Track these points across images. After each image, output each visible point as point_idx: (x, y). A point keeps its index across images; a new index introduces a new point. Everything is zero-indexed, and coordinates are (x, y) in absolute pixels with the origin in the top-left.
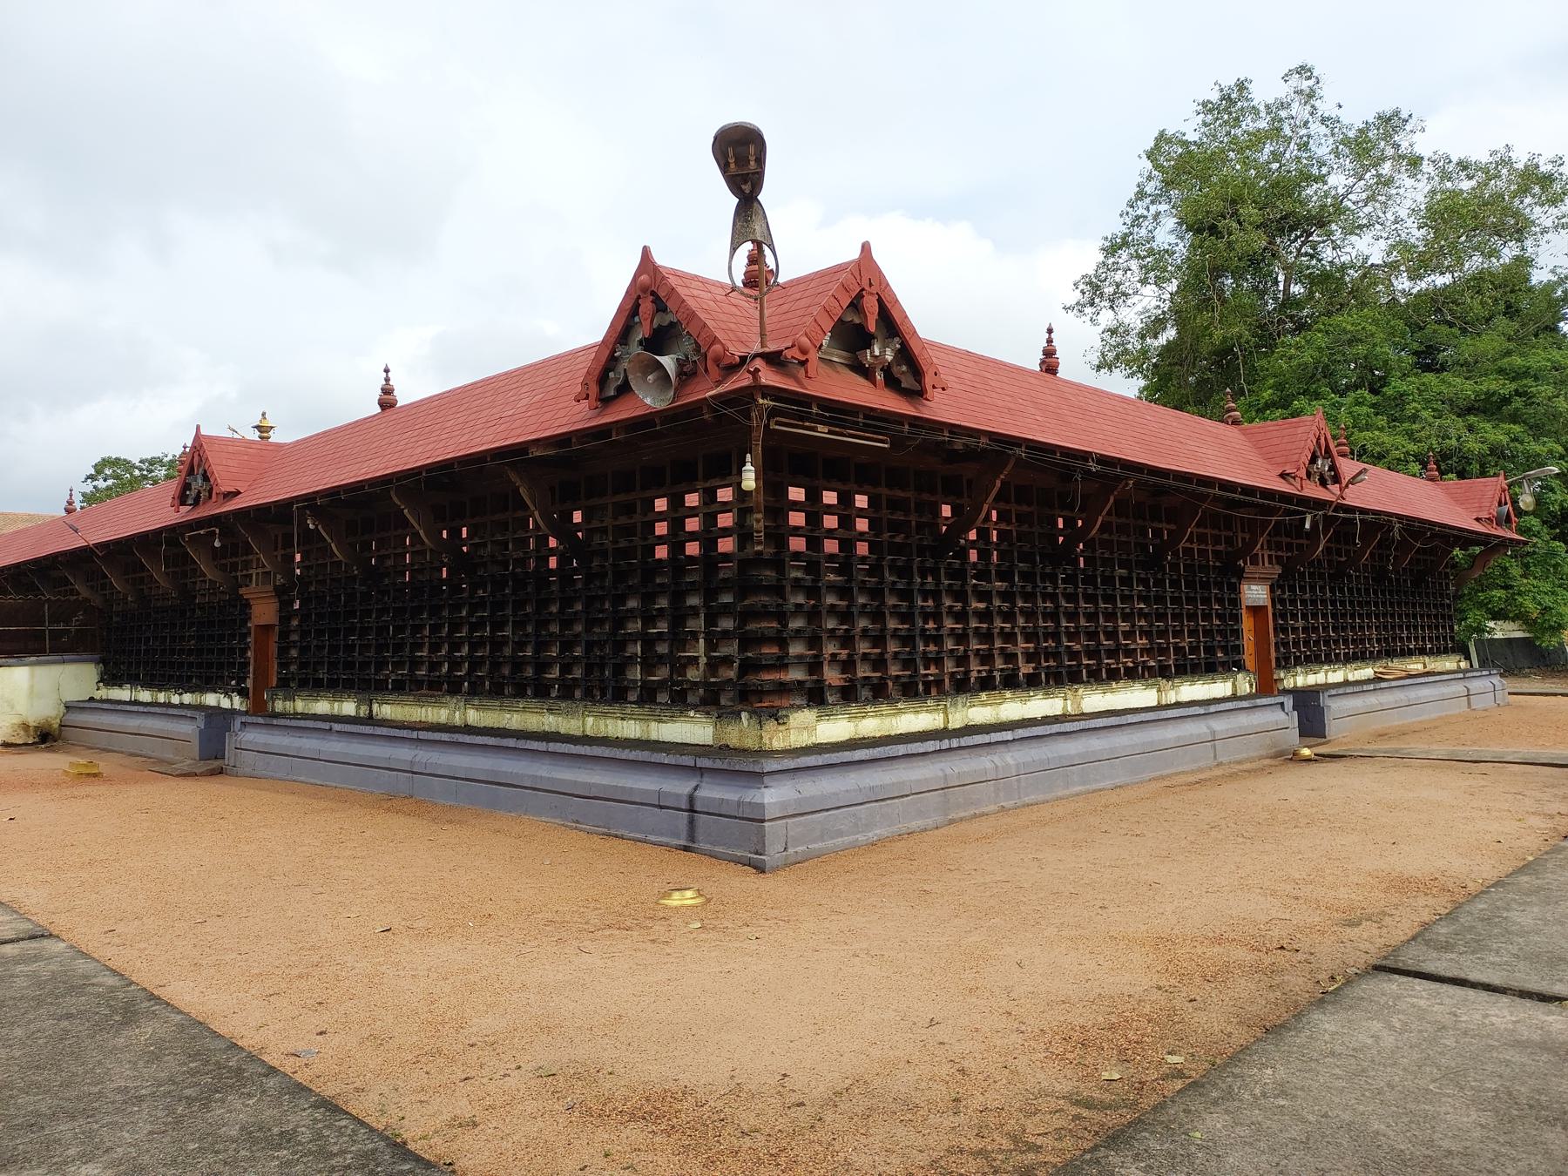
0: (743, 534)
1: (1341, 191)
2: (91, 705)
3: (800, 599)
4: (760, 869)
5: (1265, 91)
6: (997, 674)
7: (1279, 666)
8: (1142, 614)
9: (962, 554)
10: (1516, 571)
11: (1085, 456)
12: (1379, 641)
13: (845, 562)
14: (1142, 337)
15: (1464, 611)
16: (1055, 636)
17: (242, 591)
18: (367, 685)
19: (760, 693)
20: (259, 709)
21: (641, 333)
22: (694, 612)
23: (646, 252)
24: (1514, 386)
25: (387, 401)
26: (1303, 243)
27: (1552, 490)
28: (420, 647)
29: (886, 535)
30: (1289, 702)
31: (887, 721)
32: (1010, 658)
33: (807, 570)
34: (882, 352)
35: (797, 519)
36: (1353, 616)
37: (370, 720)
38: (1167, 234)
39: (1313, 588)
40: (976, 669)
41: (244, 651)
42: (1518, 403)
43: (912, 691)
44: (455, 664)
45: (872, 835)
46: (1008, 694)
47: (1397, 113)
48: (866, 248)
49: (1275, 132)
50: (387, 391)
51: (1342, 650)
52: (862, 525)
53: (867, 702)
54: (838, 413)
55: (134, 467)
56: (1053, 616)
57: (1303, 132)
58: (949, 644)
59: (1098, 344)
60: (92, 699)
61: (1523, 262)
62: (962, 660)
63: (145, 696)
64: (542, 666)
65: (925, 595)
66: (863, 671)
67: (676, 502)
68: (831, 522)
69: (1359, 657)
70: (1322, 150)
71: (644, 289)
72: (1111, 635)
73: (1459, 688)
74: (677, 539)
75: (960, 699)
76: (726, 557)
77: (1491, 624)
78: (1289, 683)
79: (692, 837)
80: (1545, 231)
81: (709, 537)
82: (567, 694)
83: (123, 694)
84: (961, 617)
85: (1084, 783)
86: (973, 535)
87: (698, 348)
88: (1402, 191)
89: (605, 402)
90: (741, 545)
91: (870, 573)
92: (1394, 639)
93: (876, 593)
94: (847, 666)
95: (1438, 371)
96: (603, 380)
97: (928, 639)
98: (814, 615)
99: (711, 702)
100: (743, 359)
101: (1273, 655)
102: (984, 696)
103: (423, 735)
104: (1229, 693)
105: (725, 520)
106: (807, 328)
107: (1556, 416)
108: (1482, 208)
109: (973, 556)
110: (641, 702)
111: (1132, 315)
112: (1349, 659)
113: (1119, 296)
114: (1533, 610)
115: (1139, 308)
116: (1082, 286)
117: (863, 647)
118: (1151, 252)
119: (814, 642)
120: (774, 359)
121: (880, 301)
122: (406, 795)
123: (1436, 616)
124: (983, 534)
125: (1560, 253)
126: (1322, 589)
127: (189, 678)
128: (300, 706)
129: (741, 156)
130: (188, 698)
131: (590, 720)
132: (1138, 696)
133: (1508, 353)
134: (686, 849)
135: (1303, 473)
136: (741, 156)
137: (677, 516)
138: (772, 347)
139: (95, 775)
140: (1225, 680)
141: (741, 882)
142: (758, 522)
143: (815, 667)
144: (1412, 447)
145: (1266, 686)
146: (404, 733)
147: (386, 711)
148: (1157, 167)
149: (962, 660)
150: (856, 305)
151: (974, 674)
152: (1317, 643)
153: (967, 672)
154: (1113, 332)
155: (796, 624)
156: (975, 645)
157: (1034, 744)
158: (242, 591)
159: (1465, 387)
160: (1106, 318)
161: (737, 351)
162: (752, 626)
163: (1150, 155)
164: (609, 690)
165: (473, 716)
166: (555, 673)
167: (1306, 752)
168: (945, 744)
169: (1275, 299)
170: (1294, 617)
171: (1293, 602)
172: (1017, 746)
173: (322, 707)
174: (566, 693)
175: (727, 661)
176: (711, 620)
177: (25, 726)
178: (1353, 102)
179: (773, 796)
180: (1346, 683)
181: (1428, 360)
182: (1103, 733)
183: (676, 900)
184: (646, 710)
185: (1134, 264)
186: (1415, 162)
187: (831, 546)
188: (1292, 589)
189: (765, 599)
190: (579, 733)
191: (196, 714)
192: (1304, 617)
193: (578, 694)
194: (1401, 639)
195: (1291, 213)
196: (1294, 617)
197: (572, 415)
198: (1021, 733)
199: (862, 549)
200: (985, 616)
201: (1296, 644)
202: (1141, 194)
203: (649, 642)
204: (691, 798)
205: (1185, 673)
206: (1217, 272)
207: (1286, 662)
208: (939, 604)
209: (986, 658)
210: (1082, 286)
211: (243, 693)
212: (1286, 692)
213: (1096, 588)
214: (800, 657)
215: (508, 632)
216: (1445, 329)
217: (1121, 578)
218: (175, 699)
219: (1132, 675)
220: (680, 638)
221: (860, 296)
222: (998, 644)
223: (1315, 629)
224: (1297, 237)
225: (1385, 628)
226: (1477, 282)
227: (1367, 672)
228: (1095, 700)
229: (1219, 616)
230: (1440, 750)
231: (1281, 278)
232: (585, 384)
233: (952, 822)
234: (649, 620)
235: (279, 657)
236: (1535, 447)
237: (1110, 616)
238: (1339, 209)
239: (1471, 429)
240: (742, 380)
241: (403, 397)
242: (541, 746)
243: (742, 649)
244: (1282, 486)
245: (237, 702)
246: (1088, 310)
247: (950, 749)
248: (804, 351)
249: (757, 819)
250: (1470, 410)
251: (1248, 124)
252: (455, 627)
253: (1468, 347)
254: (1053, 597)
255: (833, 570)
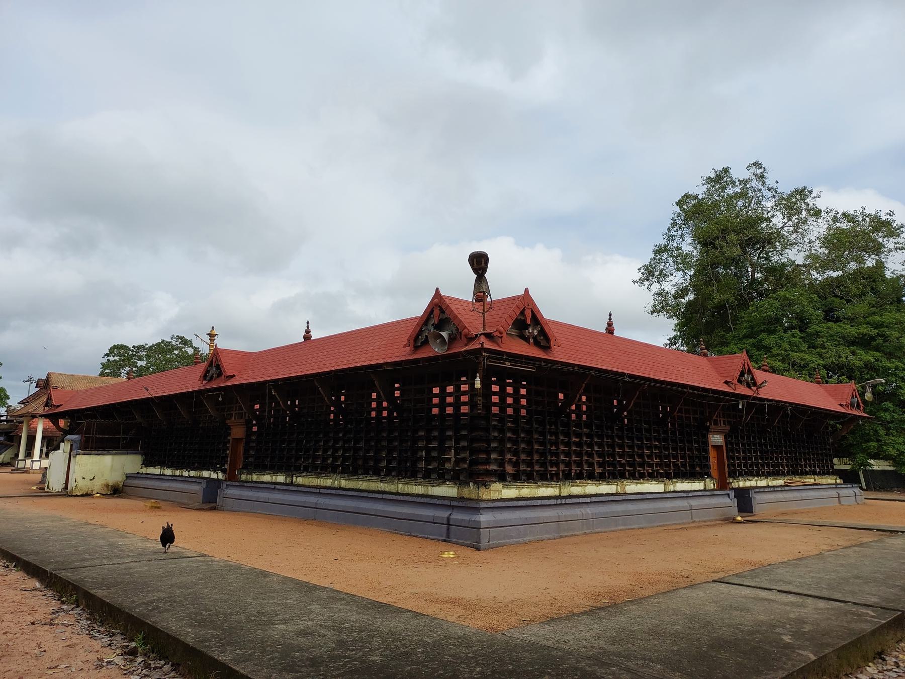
0: (472, 404)
1: (780, 225)
2: (138, 476)
3: (496, 434)
4: (478, 549)
5: (739, 173)
6: (584, 472)
7: (730, 476)
8: (656, 447)
9: (568, 416)
10: (882, 432)
11: (623, 374)
12: (787, 466)
13: (516, 416)
14: (675, 297)
15: (855, 454)
16: (613, 455)
17: (228, 421)
18: (290, 468)
19: (479, 474)
20: (232, 477)
21: (435, 320)
22: (450, 438)
23: (437, 290)
24: (876, 331)
25: (307, 337)
26: (761, 252)
27: (901, 388)
28: (317, 451)
29: (534, 407)
30: (732, 494)
31: (533, 490)
32: (591, 465)
33: (499, 421)
34: (533, 331)
35: (495, 399)
36: (772, 453)
37: (292, 484)
38: (688, 246)
39: (748, 438)
40: (574, 469)
41: (225, 451)
42: (880, 340)
43: (545, 478)
44: (335, 459)
45: (526, 539)
46: (589, 482)
47: (804, 189)
48: (527, 290)
49: (743, 194)
50: (308, 332)
51: (766, 469)
52: (523, 402)
53: (524, 481)
54: (515, 358)
55: (129, 350)
56: (612, 446)
57: (759, 194)
58: (562, 457)
59: (652, 302)
60: (138, 473)
61: (880, 266)
62: (568, 465)
63: (168, 472)
64: (378, 460)
65: (551, 434)
66: (523, 467)
67: (443, 390)
68: (510, 400)
69: (776, 474)
70: (769, 204)
71: (436, 305)
72: (641, 456)
73: (833, 493)
74: (442, 405)
75: (567, 483)
76: (465, 415)
77: (871, 461)
78: (735, 485)
79: (448, 536)
80: (890, 251)
81: (457, 405)
82: (389, 474)
83: (157, 471)
84: (568, 444)
85: (625, 525)
86: (573, 407)
87: (457, 329)
88: (811, 227)
89: (416, 348)
90: (471, 409)
91: (526, 423)
92: (797, 466)
93: (529, 432)
94: (516, 465)
95: (835, 322)
96: (416, 339)
97: (552, 454)
98: (501, 441)
99: (456, 478)
100: (476, 335)
101: (727, 470)
102: (578, 482)
103: (322, 491)
104: (702, 488)
105: (464, 398)
106: (503, 322)
107: (900, 348)
108: (860, 236)
109: (574, 416)
110: (424, 478)
111: (670, 286)
112: (769, 475)
113: (663, 277)
114: (893, 452)
115: (673, 283)
116: (642, 271)
117: (523, 457)
118: (680, 255)
119: (502, 453)
120: (489, 336)
121: (532, 311)
122: (313, 516)
123: (822, 455)
124: (579, 407)
125: (897, 263)
126: (754, 438)
127: (193, 463)
128: (255, 477)
129: (479, 262)
130: (192, 473)
131: (400, 486)
132: (654, 487)
133: (874, 313)
134: (445, 541)
135: (736, 381)
136: (479, 262)
137: (443, 395)
138: (488, 331)
139: (158, 508)
140: (700, 481)
141: (471, 553)
142: (479, 400)
143: (501, 464)
144: (821, 362)
145: (723, 485)
146: (313, 490)
147: (300, 480)
148: (683, 210)
149: (568, 465)
150: (522, 313)
151: (573, 471)
152: (751, 465)
153: (570, 470)
154: (660, 294)
155: (494, 445)
156: (574, 458)
157: (601, 505)
158: (228, 421)
159: (851, 330)
160: (656, 287)
161: (474, 332)
162: (475, 445)
163: (678, 204)
164: (410, 473)
165: (344, 483)
166: (384, 464)
167: (739, 518)
168: (559, 502)
169: (747, 280)
170: (738, 452)
171: (737, 444)
172: (591, 505)
173: (267, 478)
174: (391, 473)
175: (464, 460)
176: (457, 442)
177: (107, 485)
178: (784, 179)
179: (484, 518)
180: (768, 486)
181: (829, 315)
182: (635, 502)
183: (446, 555)
184: (427, 481)
185: (670, 260)
186: (817, 213)
187: (510, 411)
188: (737, 437)
189: (481, 433)
190: (395, 491)
191: (202, 481)
192: (744, 452)
193: (394, 473)
194: (801, 466)
195: (754, 236)
196: (738, 452)
197: (400, 353)
198: (594, 499)
199: (523, 412)
200: (579, 445)
201: (740, 466)
202: (674, 224)
203: (429, 451)
204: (448, 519)
205: (679, 477)
206: (714, 265)
207: (734, 474)
208: (557, 438)
209: (579, 464)
210: (642, 271)
211: (224, 471)
212: (733, 489)
213: (633, 433)
214: (495, 459)
215: (362, 444)
216: (837, 300)
217: (645, 429)
218: (186, 474)
219: (652, 476)
220: (443, 450)
221: (524, 309)
222: (585, 458)
223: (750, 459)
224: (758, 249)
225: (791, 460)
226: (855, 276)
227: (780, 482)
228: (632, 487)
229: (697, 450)
230: (806, 520)
231: (750, 269)
232: (408, 340)
233: (561, 537)
234: (429, 441)
235: (244, 454)
236: (888, 364)
237: (640, 447)
238: (778, 233)
239: (853, 353)
240: (475, 346)
241: (315, 335)
242: (380, 496)
243: (471, 455)
244: (726, 389)
245: (221, 476)
246: (646, 283)
247: (561, 504)
248: (501, 333)
249: (477, 527)
250: (853, 343)
251: (730, 191)
252: (336, 442)
253: (845, 310)
254: (612, 437)
255: (510, 422)
